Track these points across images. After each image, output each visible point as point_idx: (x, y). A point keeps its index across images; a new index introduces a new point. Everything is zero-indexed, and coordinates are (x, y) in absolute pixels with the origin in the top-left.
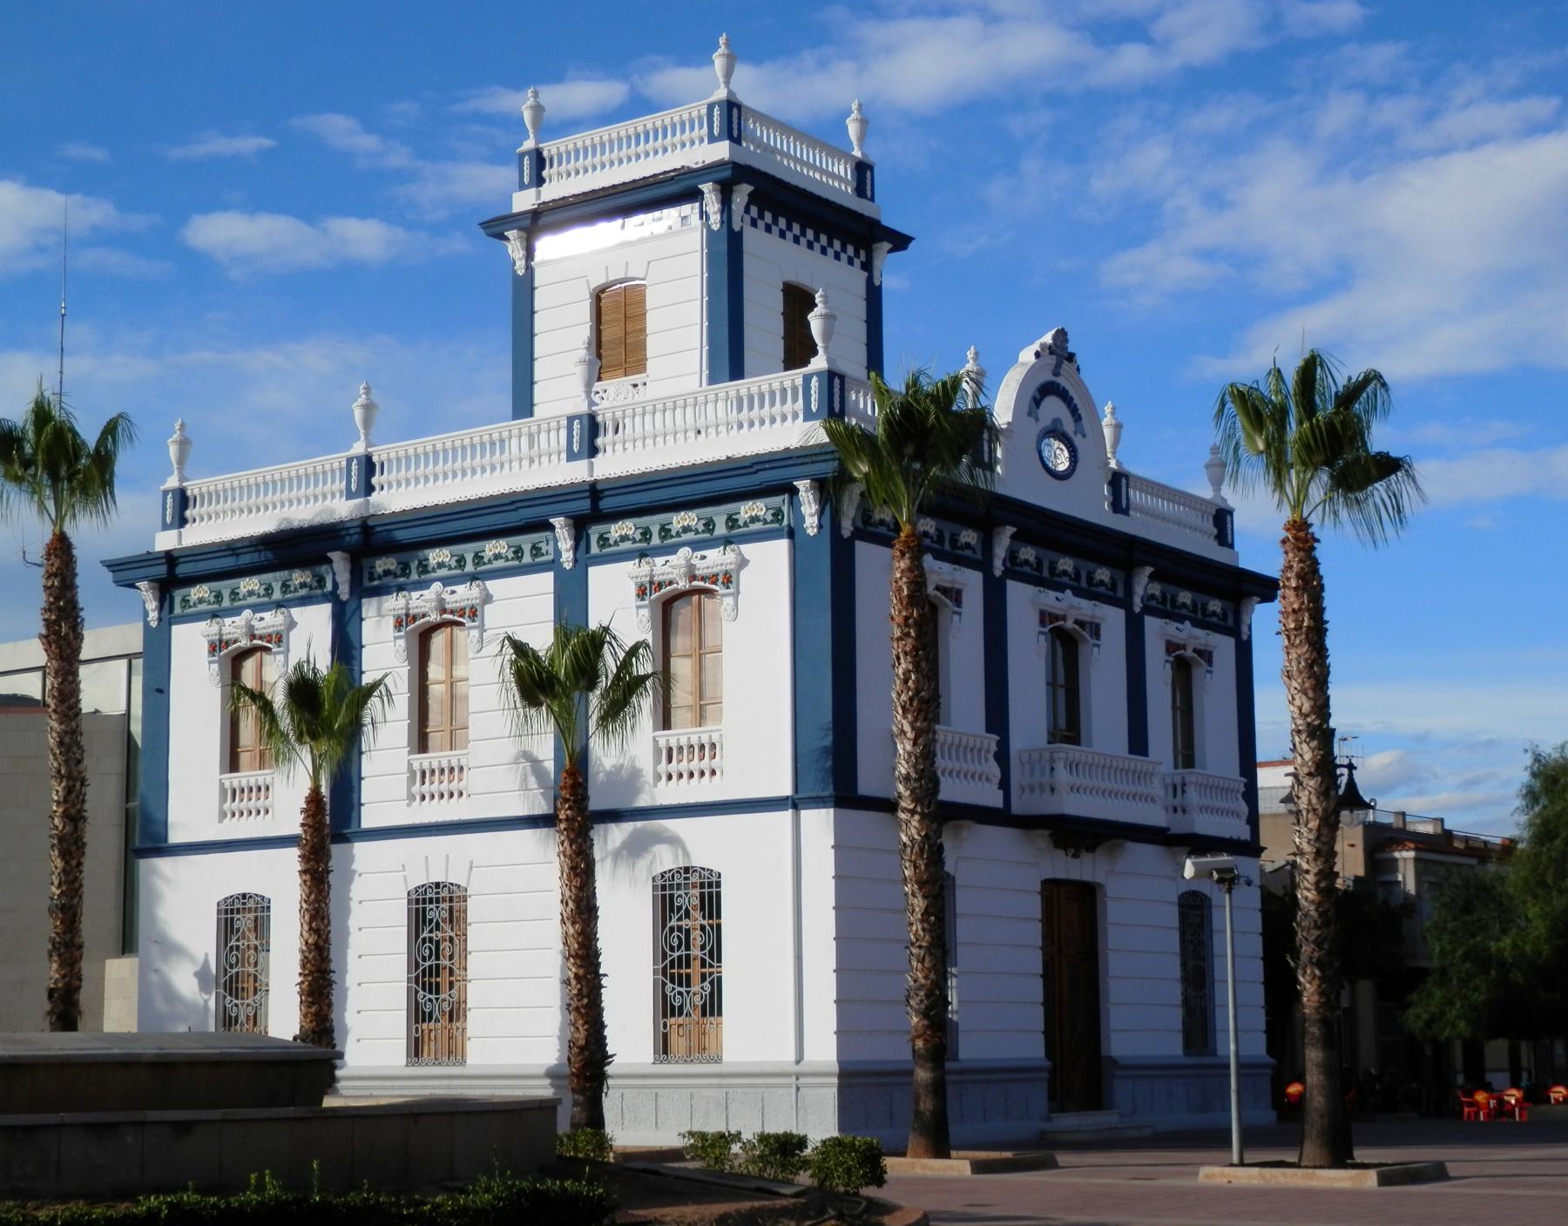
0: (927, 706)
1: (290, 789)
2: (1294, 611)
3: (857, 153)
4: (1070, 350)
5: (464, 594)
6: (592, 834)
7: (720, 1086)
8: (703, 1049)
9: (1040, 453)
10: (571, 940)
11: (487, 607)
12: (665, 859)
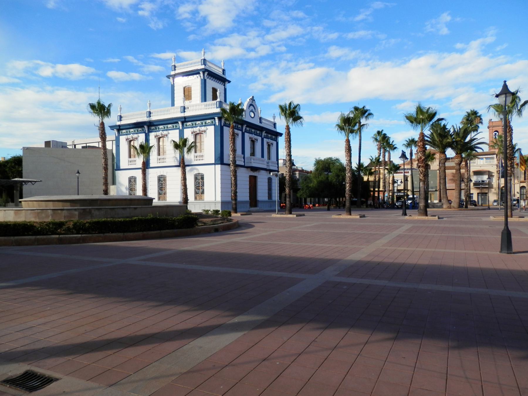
0: (234, 151)
1: (139, 161)
5: (165, 133)
8: (201, 199)
12: (196, 172)
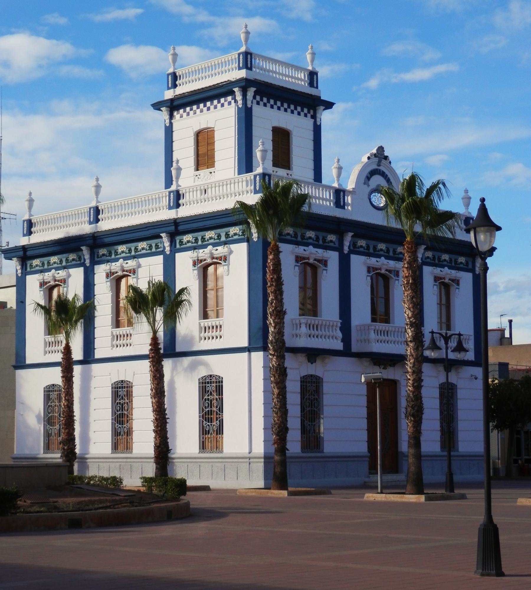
1: (141, 336)
2: (406, 277)
3: (310, 68)
4: (385, 155)
5: (131, 264)
6: (163, 363)
7: (222, 462)
8: (218, 447)
9: (370, 199)
10: (154, 404)
11: (139, 269)
12: (203, 372)
